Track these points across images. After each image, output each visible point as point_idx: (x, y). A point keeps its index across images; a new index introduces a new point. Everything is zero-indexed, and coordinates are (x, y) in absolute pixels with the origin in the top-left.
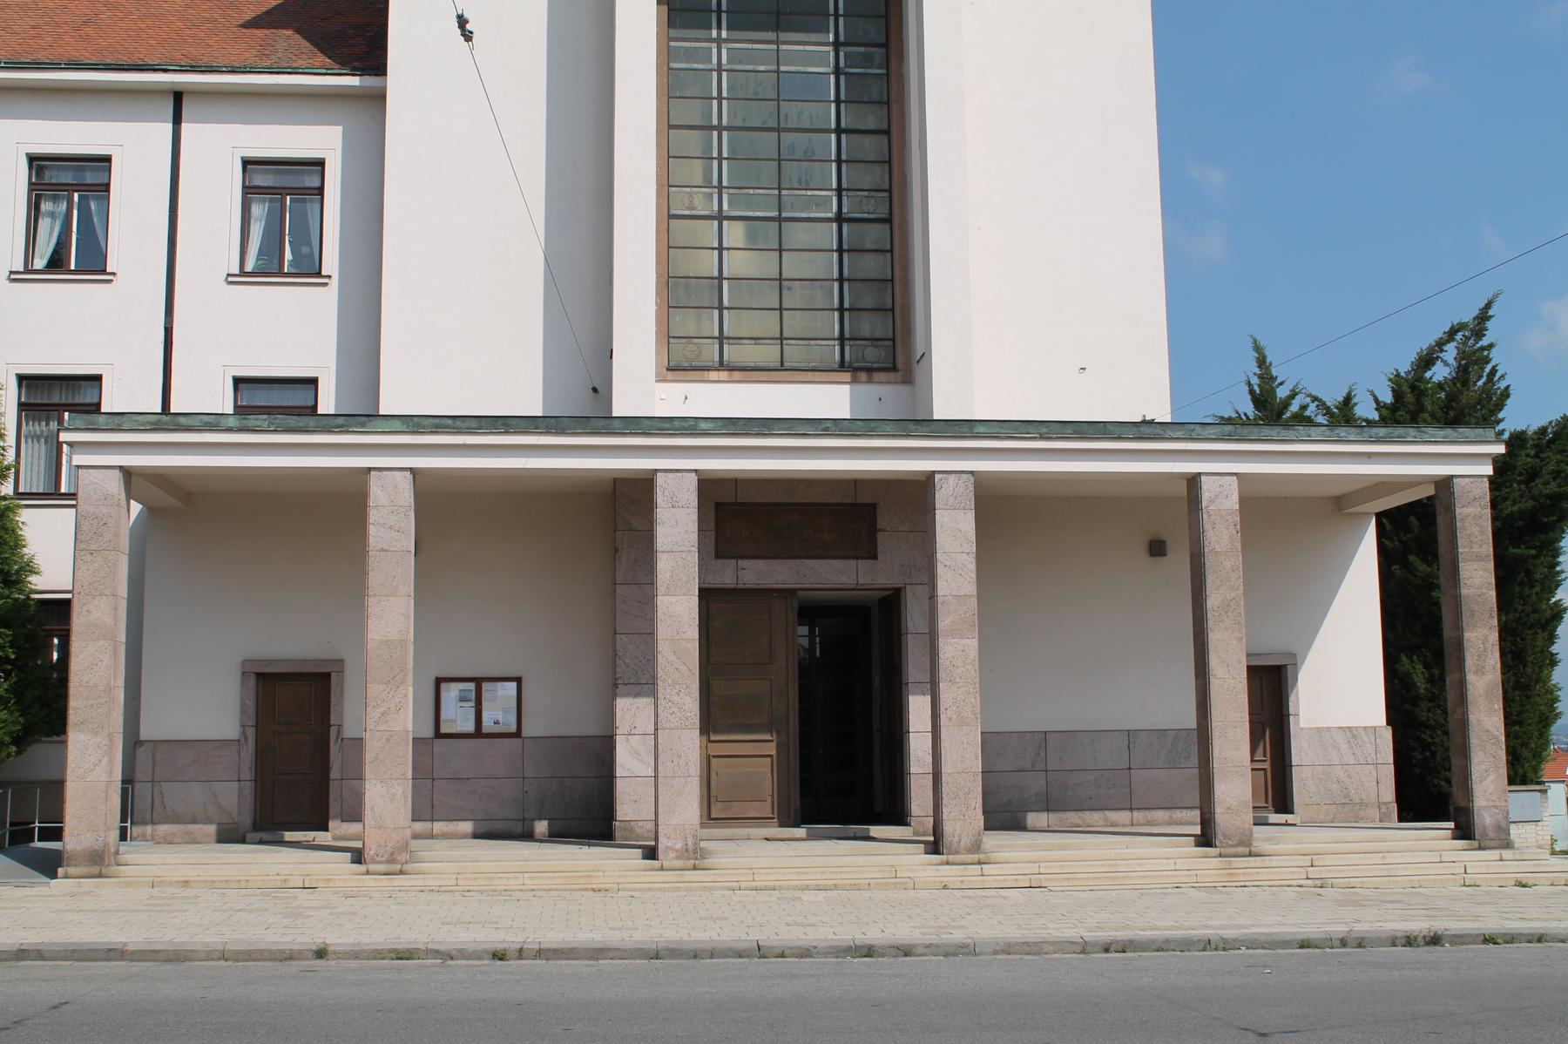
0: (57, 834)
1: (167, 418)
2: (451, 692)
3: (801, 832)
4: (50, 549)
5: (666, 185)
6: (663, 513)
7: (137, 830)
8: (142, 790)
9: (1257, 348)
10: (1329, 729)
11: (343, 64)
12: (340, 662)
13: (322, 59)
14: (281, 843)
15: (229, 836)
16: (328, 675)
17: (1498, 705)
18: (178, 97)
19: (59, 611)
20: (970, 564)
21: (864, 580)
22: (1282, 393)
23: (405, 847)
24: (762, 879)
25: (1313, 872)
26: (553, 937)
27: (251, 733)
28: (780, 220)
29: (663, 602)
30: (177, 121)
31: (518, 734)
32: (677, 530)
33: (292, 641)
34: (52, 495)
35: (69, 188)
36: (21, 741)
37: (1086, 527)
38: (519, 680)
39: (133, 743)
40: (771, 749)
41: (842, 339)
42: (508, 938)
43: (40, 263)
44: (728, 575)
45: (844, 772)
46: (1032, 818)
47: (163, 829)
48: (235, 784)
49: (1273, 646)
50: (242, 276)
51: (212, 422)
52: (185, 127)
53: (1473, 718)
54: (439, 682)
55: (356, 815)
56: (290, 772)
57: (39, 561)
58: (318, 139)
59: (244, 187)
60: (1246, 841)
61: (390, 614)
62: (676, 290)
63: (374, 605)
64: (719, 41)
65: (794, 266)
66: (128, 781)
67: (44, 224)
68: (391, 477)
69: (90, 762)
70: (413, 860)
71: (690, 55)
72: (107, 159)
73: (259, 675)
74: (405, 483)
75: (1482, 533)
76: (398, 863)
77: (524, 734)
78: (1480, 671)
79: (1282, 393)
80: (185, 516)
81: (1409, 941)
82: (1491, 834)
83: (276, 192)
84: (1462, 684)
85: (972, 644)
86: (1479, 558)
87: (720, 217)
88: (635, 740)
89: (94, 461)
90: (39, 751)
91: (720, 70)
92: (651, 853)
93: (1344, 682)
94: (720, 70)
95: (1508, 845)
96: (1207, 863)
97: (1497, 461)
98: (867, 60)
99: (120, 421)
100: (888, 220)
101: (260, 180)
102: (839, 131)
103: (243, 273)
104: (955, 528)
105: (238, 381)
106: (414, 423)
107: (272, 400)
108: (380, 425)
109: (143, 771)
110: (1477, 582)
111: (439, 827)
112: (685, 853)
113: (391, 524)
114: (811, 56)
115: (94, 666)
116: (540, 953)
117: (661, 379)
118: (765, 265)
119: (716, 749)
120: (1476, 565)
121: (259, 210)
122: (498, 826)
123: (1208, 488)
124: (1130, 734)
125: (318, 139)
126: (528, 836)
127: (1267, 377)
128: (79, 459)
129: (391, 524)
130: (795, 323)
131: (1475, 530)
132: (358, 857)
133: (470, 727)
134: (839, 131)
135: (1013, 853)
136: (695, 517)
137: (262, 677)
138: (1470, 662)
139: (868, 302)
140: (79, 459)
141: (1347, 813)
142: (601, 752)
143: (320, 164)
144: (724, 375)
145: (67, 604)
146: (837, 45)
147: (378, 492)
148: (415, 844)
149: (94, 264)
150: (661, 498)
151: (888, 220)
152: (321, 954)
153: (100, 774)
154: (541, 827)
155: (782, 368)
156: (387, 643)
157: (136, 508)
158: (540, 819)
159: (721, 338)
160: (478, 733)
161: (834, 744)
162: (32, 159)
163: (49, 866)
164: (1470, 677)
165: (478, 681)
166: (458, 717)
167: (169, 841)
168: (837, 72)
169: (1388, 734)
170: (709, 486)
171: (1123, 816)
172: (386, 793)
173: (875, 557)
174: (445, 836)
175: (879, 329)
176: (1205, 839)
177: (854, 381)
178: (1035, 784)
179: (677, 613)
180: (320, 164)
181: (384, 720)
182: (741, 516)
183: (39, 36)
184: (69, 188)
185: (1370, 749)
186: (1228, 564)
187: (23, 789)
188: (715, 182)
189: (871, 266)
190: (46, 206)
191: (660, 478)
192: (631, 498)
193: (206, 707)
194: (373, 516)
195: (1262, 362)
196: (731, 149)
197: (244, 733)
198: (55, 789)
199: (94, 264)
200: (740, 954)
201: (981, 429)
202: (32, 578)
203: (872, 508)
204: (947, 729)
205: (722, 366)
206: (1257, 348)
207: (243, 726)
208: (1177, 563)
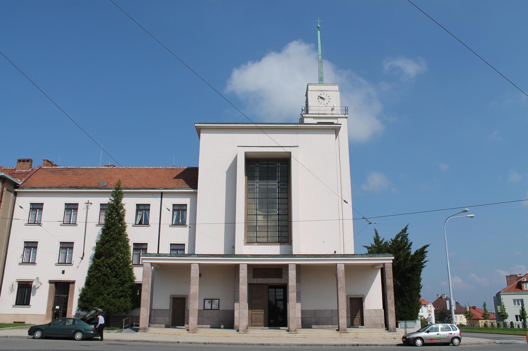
0: (138, 325)
1: (158, 255)
2: (207, 302)
4: (139, 274)
5: (247, 209)
6: (241, 271)
7: (151, 325)
8: (152, 318)
9: (375, 230)
12: (187, 296)
13: (187, 186)
15: (167, 326)
17: (394, 305)
18: (162, 193)
19: (140, 286)
21: (280, 282)
22: (381, 240)
23: (196, 328)
25: (356, 336)
26: (210, 342)
28: (267, 215)
29: (241, 286)
30: (162, 198)
31: (219, 309)
32: (243, 274)
33: (179, 292)
34: (138, 265)
35: (143, 210)
36: (133, 308)
37: (317, 272)
39: (151, 309)
40: (263, 313)
41: (279, 237)
42: (207, 341)
43: (138, 223)
44: (255, 281)
45: (277, 318)
46: (313, 326)
47: (156, 325)
49: (356, 292)
50: (173, 225)
51: (165, 255)
53: (389, 308)
54: (205, 299)
55: (188, 324)
56: (178, 316)
57: (136, 277)
58: (186, 201)
60: (345, 330)
63: (192, 287)
64: (257, 182)
65: (269, 224)
66: (150, 316)
67: (138, 216)
68: (195, 264)
69: (144, 313)
70: (197, 331)
71: (252, 185)
72: (149, 205)
74: (197, 266)
76: (194, 331)
78: (390, 299)
79: (381, 240)
80: (160, 270)
81: (353, 345)
83: (178, 210)
86: (390, 278)
87: (257, 215)
89: (147, 261)
90: (135, 311)
92: (238, 331)
93: (373, 301)
95: (395, 331)
96: (337, 334)
97: (393, 260)
98: (284, 185)
99: (151, 255)
100: (287, 215)
102: (278, 198)
103: (172, 225)
104: (292, 274)
105: (171, 244)
106: (199, 256)
107: (177, 249)
108: (193, 256)
109: (153, 315)
111: (204, 326)
112: (243, 331)
113: (195, 272)
114: (274, 184)
115: (145, 296)
116: (212, 343)
117: (245, 245)
119: (253, 313)
121: (175, 213)
122: (215, 326)
123: (338, 266)
124: (332, 310)
125: (186, 201)
126: (220, 328)
127: (377, 236)
128: (144, 261)
129: (195, 272)
130: (270, 234)
132: (188, 330)
133: (210, 308)
134: (278, 198)
136: (247, 272)
137: (174, 298)
139: (284, 230)
140: (144, 261)
141: (375, 326)
142: (232, 313)
143: (186, 205)
145: (141, 284)
146: (278, 182)
147: (193, 267)
149: (147, 224)
151: (287, 215)
152: (178, 342)
153: (146, 315)
154: (222, 326)
155: (268, 242)
157: (153, 268)
159: (257, 237)
160: (211, 309)
162: (137, 205)
163: (137, 330)
165: (212, 300)
166: (208, 306)
167: (157, 327)
168: (278, 187)
170: (249, 266)
171: (331, 326)
172: (193, 319)
174: (205, 328)
175: (284, 236)
176: (338, 330)
177: (281, 245)
178: (314, 320)
180: (186, 205)
181: (194, 306)
184: (143, 210)
187: (132, 317)
189: (284, 223)
190: (139, 213)
192: (237, 267)
193: (164, 304)
194: (192, 271)
195: (376, 233)
198: (138, 318)
199: (147, 224)
200: (243, 344)
202: (135, 280)
203: (281, 269)
204: (295, 310)
205: (257, 242)
206: (375, 230)
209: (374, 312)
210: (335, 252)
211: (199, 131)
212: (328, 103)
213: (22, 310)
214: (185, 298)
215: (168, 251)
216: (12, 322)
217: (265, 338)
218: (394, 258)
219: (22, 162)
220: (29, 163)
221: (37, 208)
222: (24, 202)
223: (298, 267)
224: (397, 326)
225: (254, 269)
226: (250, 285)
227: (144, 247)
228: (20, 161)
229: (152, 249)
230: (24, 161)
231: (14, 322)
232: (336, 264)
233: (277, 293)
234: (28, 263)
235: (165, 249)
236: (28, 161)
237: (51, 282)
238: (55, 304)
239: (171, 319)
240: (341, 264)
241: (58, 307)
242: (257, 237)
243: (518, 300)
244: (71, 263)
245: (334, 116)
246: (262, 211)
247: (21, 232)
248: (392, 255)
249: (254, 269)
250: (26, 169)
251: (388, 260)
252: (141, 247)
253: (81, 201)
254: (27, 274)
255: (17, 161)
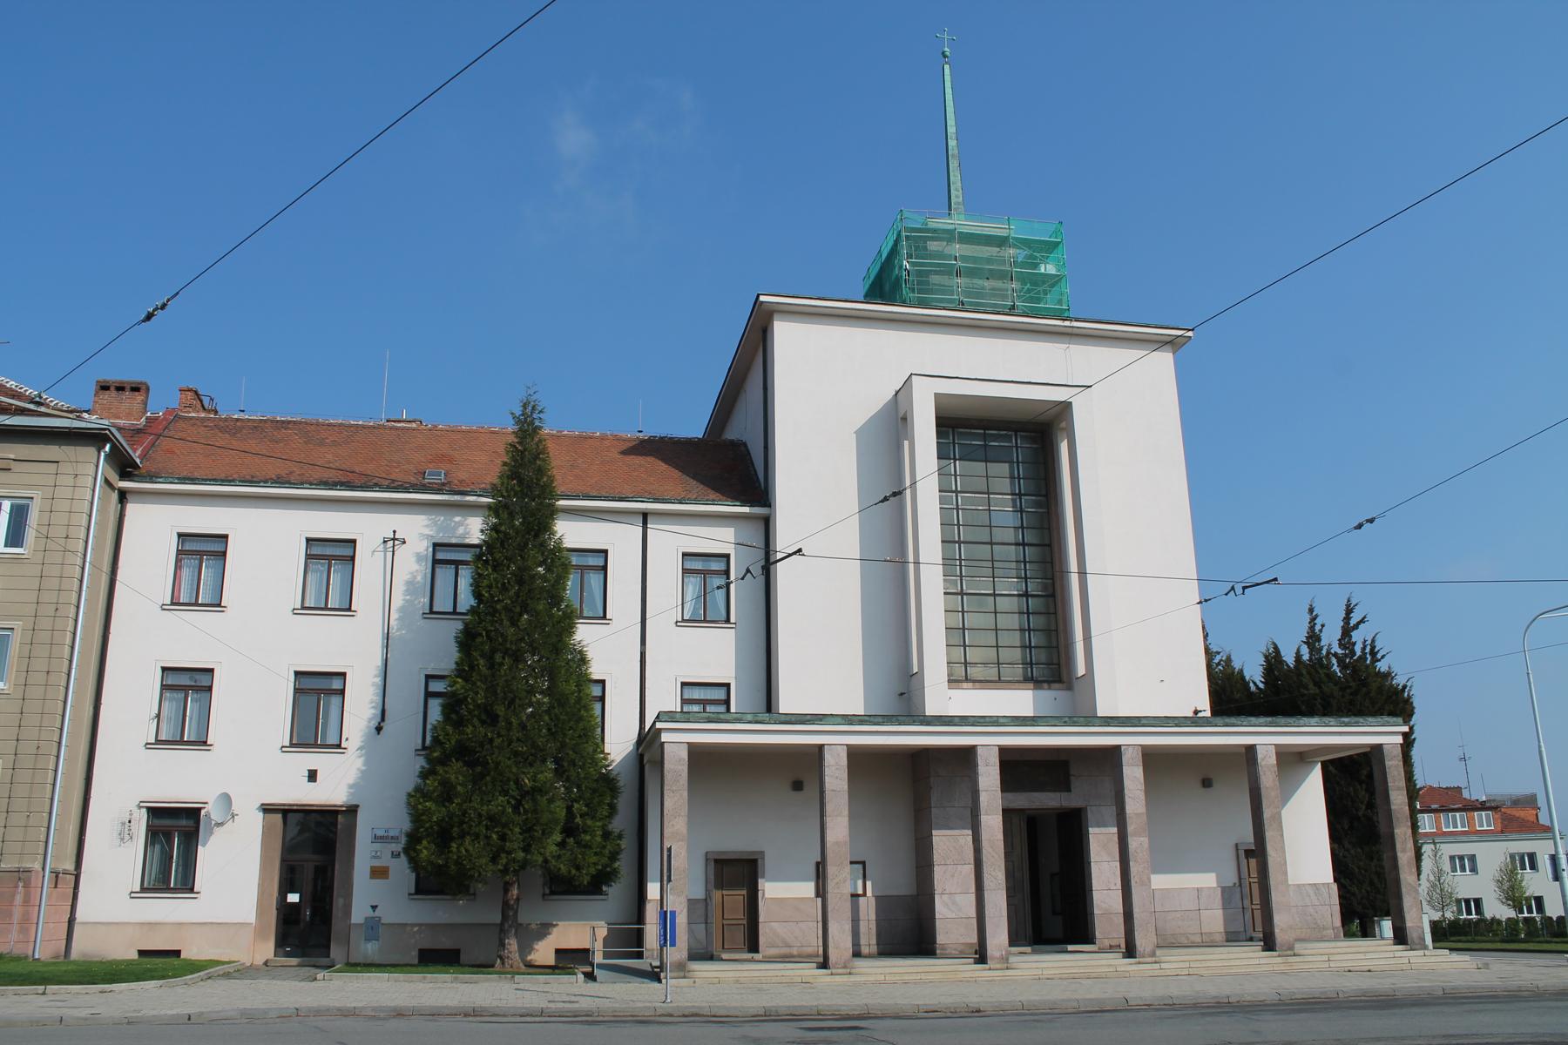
3: (294, 961)
11: (716, 489)
13: (713, 495)
14: (1067, 952)
18: (645, 516)
20: (1142, 796)
30: (645, 523)
38: (863, 863)
44: (1023, 800)
50: (684, 622)
53: (1402, 876)
58: (720, 539)
62: (958, 635)
72: (226, 537)
78: (1404, 851)
84: (1395, 859)
85: (1145, 840)
86: (1399, 789)
88: (945, 897)
101: (316, 550)
103: (683, 620)
118: (987, 621)
125: (720, 539)
135: (702, 969)
138: (1398, 846)
141: (1112, 949)
144: (970, 685)
147: (828, 757)
148: (1158, 952)
156: (837, 843)
161: (1052, 904)
164: (1399, 855)
169: (1335, 887)
170: (1004, 751)
173: (1069, 790)
182: (1020, 768)
185: (1326, 895)
205: (967, 680)
208: (810, 790)
209: (1311, 892)
213: (167, 909)
216: (135, 956)
219: (113, 393)
220: (139, 397)
221: (203, 551)
222: (154, 528)
227: (203, 680)
228: (104, 387)
230: (120, 389)
231: (142, 953)
232: (821, 747)
234: (179, 742)
236: (136, 389)
237: (267, 809)
238: (287, 885)
241: (293, 898)
242: (966, 663)
243: (1461, 858)
244: (205, 743)
247: (149, 635)
248: (1400, 720)
250: (128, 416)
253: (366, 528)
254: (179, 779)
255: (93, 387)
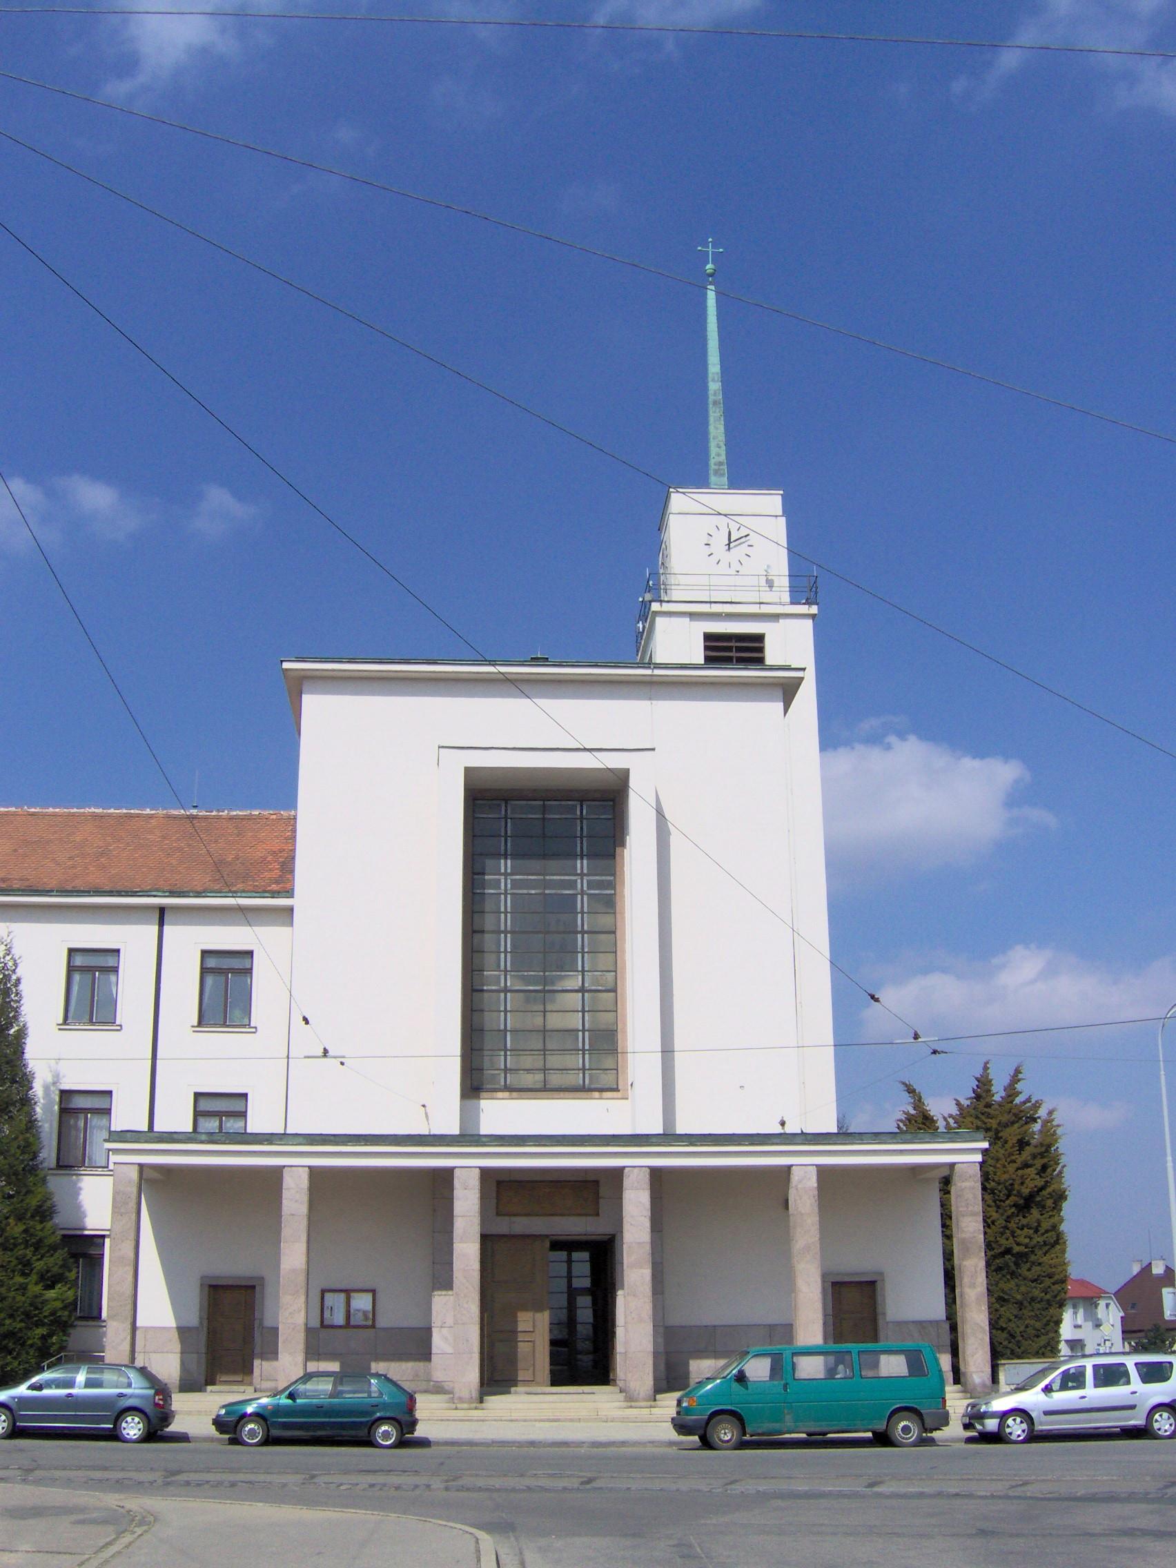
4: (95, 1201)
10: (906, 1323)
16: (253, 1287)
17: (985, 1308)
18: (162, 910)
19: (97, 1240)
24: (515, 1415)
27: (205, 1323)
30: (161, 924)
31: (373, 1326)
32: (467, 1203)
33: (232, 1264)
37: (718, 1197)
38: (373, 1292)
44: (503, 1226)
48: (195, 1356)
52: (165, 927)
54: (323, 1292)
59: (202, 968)
61: (293, 1255)
68: (296, 1168)
73: (210, 1286)
75: (975, 1198)
77: (378, 1325)
78: (973, 1286)
82: (979, 1389)
86: (974, 1214)
88: (445, 1331)
91: (506, 894)
94: (506, 894)
97: (985, 1152)
104: (636, 1205)
110: (971, 1229)
113: (295, 1197)
120: (970, 1219)
123: (796, 1175)
129: (295, 1197)
131: (970, 1196)
136: (478, 1195)
140: (114, 1158)
144: (506, 1094)
150: (457, 1183)
158: (341, 1367)
179: (467, 1252)
183: (74, 867)
186: (809, 1221)
188: (502, 967)
191: (457, 1172)
194: (285, 1194)
196: (513, 945)
197: (201, 1323)
201: (654, 1140)
203: (596, 1182)
205: (508, 1088)
207: (201, 1318)
210: (783, 1124)
211: (297, 686)
212: (744, 560)
214: (873, 1283)
215: (185, 1124)
217: (547, 1424)
218: (986, 1145)
223: (658, 1177)
224: (995, 1379)
225: (499, 1183)
226: (487, 1240)
229: (128, 1114)
232: (790, 1167)
233: (564, 1272)
235: (176, 1115)
239: (203, 1360)
240: (804, 1167)
245: (765, 609)
246: (523, 978)
248: (981, 1135)
249: (499, 1183)
251: (966, 1155)
252: (83, 1109)
